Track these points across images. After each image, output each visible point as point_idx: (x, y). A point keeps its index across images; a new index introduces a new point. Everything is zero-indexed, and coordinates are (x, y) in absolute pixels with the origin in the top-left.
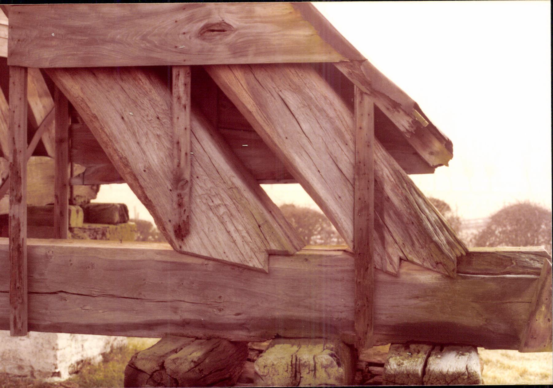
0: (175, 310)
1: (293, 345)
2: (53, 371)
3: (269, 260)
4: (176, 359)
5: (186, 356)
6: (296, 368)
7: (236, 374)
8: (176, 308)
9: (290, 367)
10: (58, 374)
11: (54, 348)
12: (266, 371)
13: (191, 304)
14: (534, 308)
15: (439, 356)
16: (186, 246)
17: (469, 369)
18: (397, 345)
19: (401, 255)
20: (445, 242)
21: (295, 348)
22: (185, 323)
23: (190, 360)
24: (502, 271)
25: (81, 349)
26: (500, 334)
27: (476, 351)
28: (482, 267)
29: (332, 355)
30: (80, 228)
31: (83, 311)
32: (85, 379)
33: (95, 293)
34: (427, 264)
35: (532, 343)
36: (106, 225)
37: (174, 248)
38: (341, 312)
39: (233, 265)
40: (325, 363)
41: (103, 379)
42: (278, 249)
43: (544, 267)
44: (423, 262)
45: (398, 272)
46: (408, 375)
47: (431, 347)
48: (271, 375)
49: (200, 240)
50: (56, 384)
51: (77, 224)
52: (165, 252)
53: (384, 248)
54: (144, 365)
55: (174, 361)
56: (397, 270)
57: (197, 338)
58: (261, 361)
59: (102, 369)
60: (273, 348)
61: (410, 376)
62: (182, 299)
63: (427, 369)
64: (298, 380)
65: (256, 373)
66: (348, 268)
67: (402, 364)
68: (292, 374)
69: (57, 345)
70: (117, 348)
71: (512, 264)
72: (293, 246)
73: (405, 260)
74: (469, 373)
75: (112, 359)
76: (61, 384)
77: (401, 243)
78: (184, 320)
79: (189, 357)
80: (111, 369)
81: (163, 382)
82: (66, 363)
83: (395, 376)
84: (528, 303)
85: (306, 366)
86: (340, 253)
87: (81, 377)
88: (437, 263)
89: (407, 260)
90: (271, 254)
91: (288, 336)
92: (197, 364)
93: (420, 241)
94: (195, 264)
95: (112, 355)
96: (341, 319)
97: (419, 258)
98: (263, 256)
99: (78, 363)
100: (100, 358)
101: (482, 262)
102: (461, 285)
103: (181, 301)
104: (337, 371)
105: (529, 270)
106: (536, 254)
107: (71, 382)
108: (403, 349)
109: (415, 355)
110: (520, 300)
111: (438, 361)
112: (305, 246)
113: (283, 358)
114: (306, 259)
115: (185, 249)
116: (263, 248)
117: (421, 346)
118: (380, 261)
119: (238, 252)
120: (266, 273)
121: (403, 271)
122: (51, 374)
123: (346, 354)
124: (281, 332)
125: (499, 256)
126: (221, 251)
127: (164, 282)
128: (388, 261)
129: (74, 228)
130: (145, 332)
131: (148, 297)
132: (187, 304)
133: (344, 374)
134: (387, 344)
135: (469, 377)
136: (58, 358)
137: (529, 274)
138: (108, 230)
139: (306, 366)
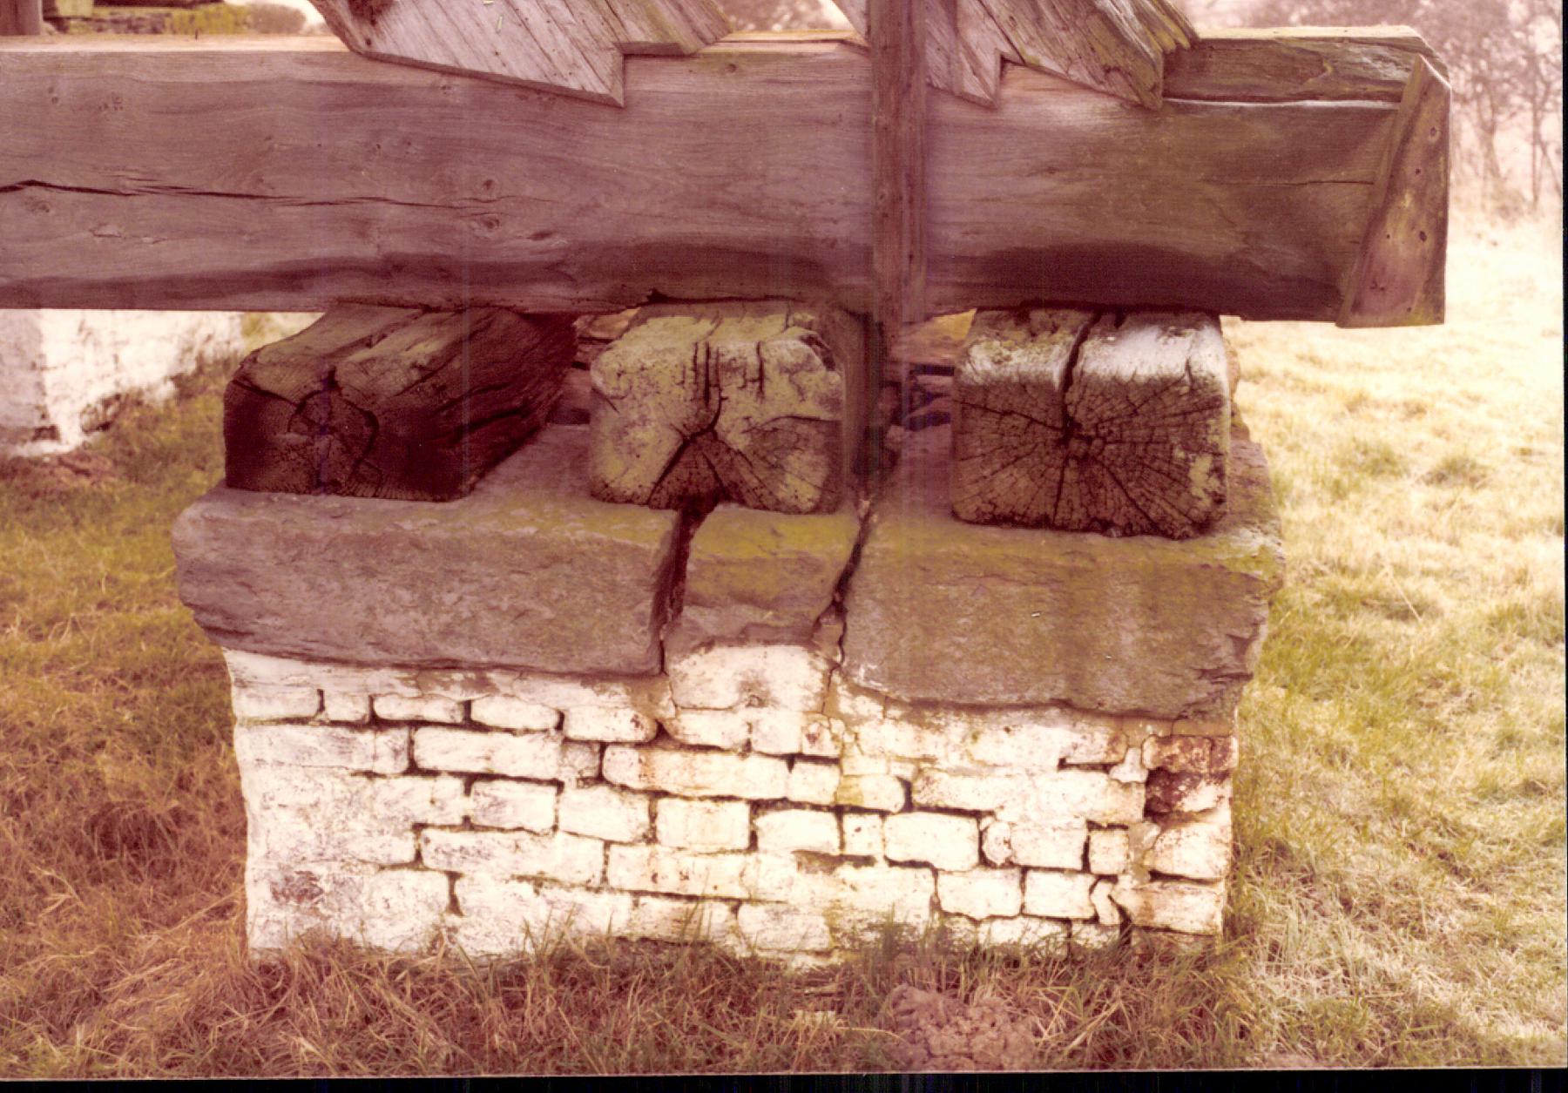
0: (362, 228)
1: (699, 318)
2: (38, 423)
3: (624, 70)
4: (368, 360)
5: (395, 352)
6: (707, 375)
7: (542, 397)
8: (367, 222)
9: (690, 373)
10: (52, 433)
11: (34, 366)
12: (624, 385)
13: (408, 209)
14: (1380, 200)
15: (1111, 339)
16: (384, 39)
17: (1195, 368)
18: (995, 313)
19: (1006, 49)
20: (1130, 13)
21: (705, 325)
22: (392, 268)
23: (408, 363)
24: (1293, 91)
25: (111, 366)
26: (1284, 279)
27: (1217, 325)
28: (1236, 81)
29: (809, 341)
30: (86, 19)
31: (98, 240)
32: (128, 444)
33: (128, 183)
34: (1079, 74)
35: (1371, 300)
36: (162, 10)
37: (350, 47)
38: (835, 222)
39: (524, 88)
40: (790, 359)
41: (180, 440)
42: (651, 40)
43: (1413, 78)
44: (1069, 66)
45: (996, 96)
46: (1024, 386)
47: (1090, 315)
48: (639, 396)
49: (423, 22)
50: (47, 460)
51: (75, 7)
52: (328, 58)
53: (956, 31)
54: (278, 380)
55: (363, 366)
56: (992, 89)
57: (427, 309)
58: (609, 360)
59: (176, 415)
60: (643, 327)
61: (1029, 389)
62: (380, 194)
63: (1077, 370)
64: (715, 407)
65: (596, 392)
66: (855, 87)
67: (1008, 359)
68: (696, 391)
69: (41, 356)
70: (216, 362)
71: (1324, 70)
72: (695, 31)
73: (1015, 64)
74: (1193, 380)
75: (204, 388)
76: (61, 460)
77: (1004, 16)
78: (388, 259)
79: (404, 354)
80: (202, 414)
81: (334, 423)
82: (73, 402)
83: (985, 389)
84: (1362, 187)
85: (735, 370)
86: (831, 48)
87: (118, 438)
88: (1107, 70)
89: (1023, 63)
90: (631, 54)
91: (685, 296)
92: (426, 372)
93: (1060, 9)
94: (410, 87)
95: (202, 379)
96: (835, 241)
97: (1055, 57)
98: (607, 62)
99: (106, 403)
100: (168, 389)
101: (1238, 68)
102: (1172, 134)
103: (377, 199)
104: (825, 379)
105: (1371, 88)
106: (1392, 44)
107: (89, 452)
108: (1012, 322)
109: (1044, 336)
110: (1343, 175)
111: (1107, 350)
112: (730, 32)
113: (671, 351)
114: (732, 65)
115: (381, 47)
116: (608, 40)
117: (1061, 313)
118: (943, 66)
119: (534, 51)
120: (620, 108)
121: (1008, 92)
122: (32, 434)
123: (849, 340)
124: (666, 286)
125: (1285, 51)
126: (486, 50)
127: (324, 142)
128: (967, 66)
129: (69, 18)
130: (280, 298)
131: (280, 192)
132: (394, 211)
133: (843, 388)
134: (966, 309)
135: (1192, 391)
136: (49, 391)
137: (1369, 97)
138: (168, 21)
139: (735, 370)
